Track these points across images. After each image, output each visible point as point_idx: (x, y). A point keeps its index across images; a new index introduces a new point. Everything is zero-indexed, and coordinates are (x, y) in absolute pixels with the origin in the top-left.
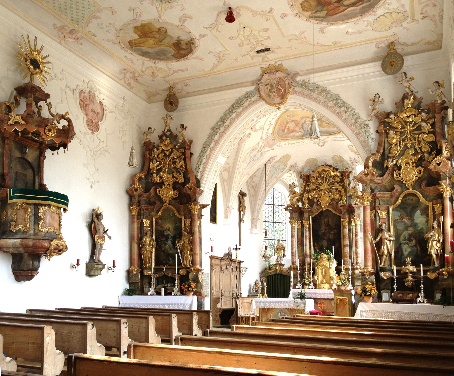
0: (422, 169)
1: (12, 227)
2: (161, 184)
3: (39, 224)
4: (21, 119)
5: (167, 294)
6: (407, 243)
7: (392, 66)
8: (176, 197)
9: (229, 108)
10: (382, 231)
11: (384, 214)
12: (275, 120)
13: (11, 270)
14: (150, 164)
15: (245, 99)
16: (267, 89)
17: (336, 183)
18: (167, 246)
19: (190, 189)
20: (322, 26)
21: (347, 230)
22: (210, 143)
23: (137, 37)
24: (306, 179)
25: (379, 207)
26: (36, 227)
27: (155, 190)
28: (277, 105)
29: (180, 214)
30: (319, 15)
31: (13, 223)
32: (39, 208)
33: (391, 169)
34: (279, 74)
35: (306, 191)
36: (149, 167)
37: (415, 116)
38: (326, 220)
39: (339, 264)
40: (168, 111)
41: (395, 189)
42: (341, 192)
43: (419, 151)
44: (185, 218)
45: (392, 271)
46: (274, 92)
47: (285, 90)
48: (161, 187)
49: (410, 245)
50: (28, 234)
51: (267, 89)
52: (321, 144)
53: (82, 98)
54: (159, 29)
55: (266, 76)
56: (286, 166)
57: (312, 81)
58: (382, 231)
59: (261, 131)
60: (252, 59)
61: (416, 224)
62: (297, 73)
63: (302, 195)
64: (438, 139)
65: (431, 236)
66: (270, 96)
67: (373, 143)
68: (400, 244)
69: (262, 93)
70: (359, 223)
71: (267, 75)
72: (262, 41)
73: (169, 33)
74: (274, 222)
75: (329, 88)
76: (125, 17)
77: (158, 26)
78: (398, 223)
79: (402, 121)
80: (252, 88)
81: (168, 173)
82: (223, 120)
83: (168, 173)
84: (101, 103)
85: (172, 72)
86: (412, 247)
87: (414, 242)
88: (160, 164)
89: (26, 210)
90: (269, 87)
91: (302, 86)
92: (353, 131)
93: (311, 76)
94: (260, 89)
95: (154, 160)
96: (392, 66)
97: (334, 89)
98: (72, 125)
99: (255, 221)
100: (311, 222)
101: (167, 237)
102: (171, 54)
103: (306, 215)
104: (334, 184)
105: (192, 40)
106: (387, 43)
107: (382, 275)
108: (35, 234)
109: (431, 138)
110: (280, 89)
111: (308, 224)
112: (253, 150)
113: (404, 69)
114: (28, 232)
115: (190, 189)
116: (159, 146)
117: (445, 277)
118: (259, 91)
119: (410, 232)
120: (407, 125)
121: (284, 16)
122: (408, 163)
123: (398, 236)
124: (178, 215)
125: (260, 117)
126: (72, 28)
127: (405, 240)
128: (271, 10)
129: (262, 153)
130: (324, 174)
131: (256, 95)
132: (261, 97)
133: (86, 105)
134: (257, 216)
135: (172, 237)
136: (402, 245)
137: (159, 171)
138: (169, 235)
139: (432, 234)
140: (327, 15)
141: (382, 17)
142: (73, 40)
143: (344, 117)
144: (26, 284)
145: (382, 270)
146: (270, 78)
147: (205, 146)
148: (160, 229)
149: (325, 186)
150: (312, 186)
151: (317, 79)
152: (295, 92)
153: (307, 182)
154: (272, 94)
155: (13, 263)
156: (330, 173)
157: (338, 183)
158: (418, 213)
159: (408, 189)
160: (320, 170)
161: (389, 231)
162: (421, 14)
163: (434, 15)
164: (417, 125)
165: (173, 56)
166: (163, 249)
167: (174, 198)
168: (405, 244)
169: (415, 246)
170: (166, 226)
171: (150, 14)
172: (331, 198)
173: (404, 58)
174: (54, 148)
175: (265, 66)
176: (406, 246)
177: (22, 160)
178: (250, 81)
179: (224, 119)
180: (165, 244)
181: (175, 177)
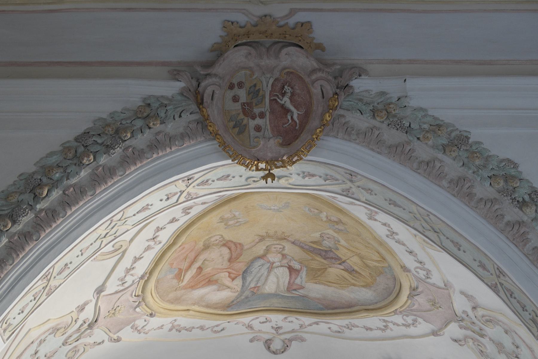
9: (66, 148)
15: (139, 123)
28: (262, 165)
34: (295, 59)
46: (262, 115)
47: (306, 117)
51: (235, 99)
52: (277, 345)
55: (238, 57)
57: (414, 103)
59: (111, 262)
62: (353, 67)
66: (241, 128)
69: (213, 112)
71: (244, 50)
75: (476, 134)
80: (170, 88)
93: (414, 84)
97: (497, 141)
110: (288, 111)
112: (55, 330)
118: (200, 103)
125: (174, 199)
129: (75, 350)
131: (187, 117)
146: (252, 64)
151: (432, 96)
152: (348, 132)
154: (252, 123)
175: (242, 19)
178: (164, 64)
179: (40, 185)
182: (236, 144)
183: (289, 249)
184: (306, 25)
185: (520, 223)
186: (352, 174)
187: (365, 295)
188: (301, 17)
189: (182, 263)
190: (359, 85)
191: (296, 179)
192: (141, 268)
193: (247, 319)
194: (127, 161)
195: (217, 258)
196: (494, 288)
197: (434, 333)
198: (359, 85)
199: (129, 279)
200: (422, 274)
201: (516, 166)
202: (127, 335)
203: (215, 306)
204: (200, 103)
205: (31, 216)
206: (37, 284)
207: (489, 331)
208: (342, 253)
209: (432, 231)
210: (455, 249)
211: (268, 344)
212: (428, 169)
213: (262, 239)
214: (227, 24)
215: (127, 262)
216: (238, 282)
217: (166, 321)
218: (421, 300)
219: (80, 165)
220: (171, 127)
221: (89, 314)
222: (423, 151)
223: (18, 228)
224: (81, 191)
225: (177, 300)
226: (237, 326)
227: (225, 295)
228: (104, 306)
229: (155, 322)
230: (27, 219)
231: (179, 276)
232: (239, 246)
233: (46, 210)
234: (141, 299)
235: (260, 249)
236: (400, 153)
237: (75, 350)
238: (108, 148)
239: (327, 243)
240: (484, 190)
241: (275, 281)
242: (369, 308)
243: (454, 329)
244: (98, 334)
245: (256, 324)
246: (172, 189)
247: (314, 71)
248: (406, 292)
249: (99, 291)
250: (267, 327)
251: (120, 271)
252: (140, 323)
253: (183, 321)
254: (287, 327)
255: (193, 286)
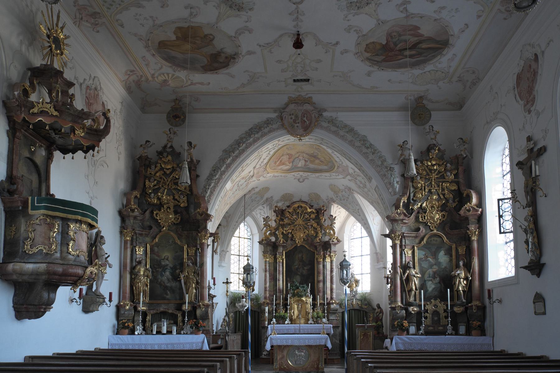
0: (446, 214)
1: (27, 247)
2: (160, 206)
3: (68, 245)
4: (52, 109)
5: (178, 333)
6: (431, 280)
7: (420, 118)
8: (178, 222)
9: (246, 133)
10: (410, 268)
11: (410, 252)
12: (273, 151)
13: (12, 305)
14: (145, 183)
15: (265, 125)
16: (291, 118)
17: (311, 220)
18: (164, 278)
19: (201, 215)
20: (372, 69)
21: (321, 266)
22: (222, 167)
23: (174, 38)
24: (280, 213)
25: (405, 245)
26: (65, 249)
27: (152, 212)
29: (181, 241)
30: (377, 58)
31: (28, 243)
32: (69, 224)
33: (416, 212)
34: (307, 107)
35: (281, 225)
36: (145, 185)
37: (439, 165)
38: (300, 256)
39: (314, 299)
40: (171, 125)
41: (421, 230)
42: (316, 229)
43: (442, 197)
44: (188, 246)
45: (420, 306)
46: (298, 123)
47: (310, 123)
48: (160, 210)
49: (434, 282)
50: (53, 257)
51: (291, 118)
52: (301, 180)
53: (88, 95)
54: (206, 36)
55: (292, 106)
56: (262, 198)
58: (410, 268)
60: (286, 87)
61: (440, 263)
63: (277, 229)
64: (462, 188)
65: (458, 274)
66: (293, 126)
67: (398, 186)
68: (425, 281)
70: (335, 259)
71: (293, 105)
72: (308, 71)
73: (214, 42)
74: (239, 256)
76: (176, 12)
77: (206, 32)
78: (423, 261)
79: (426, 168)
80: (274, 115)
81: (168, 194)
82: (238, 143)
83: (168, 194)
84: (103, 102)
85: (189, 83)
86: (436, 283)
87: (438, 279)
88: (157, 183)
89: (51, 227)
90: (293, 117)
91: (329, 122)
92: (378, 172)
94: (284, 118)
95: (152, 178)
96: (420, 118)
98: (110, 126)
99: (224, 253)
100: (284, 257)
101: (164, 268)
102: (202, 65)
103: (280, 249)
104: (309, 220)
105: (235, 55)
106: (416, 96)
107: (411, 309)
108: (62, 258)
109: (454, 187)
111: (282, 260)
113: (431, 123)
114: (53, 254)
115: (201, 215)
116: (157, 163)
117: (475, 311)
118: (282, 120)
119: (435, 270)
120: (431, 172)
121: (346, 51)
122: (434, 207)
123: (423, 272)
124: (179, 243)
126: (98, 10)
127: (429, 277)
128: (337, 43)
129: (248, 183)
130: (299, 211)
132: (283, 125)
133: (91, 104)
134: (227, 249)
135: (170, 268)
136: (427, 282)
137: (156, 191)
138: (167, 265)
139: (458, 272)
140: (384, 60)
141: (427, 73)
142: (89, 25)
143: (370, 158)
144: (29, 323)
145: (411, 304)
147: (215, 169)
148: (156, 258)
149: (300, 221)
150: (286, 221)
151: (344, 117)
152: (322, 127)
153: (281, 216)
154: (296, 125)
155: (15, 295)
156: (307, 209)
157: (313, 220)
158: (442, 253)
159: (432, 231)
160: (296, 205)
161: (414, 268)
162: (458, 77)
163: (467, 81)
164: (441, 174)
165: (202, 67)
166: (159, 280)
167: (174, 223)
168: (429, 280)
169: (439, 283)
170: (164, 255)
171: (207, 16)
172: (306, 234)
173: (432, 112)
174: (65, 151)
175: (293, 96)
176: (430, 282)
177: (29, 161)
178: (272, 108)
179: (240, 143)
180: (162, 275)
181: (176, 200)
182: (292, 133)
183: (305, 155)
184: (311, 98)
185: (367, 153)
186: (322, 139)
187: (326, 167)
188: (309, 95)
189: (276, 159)
190: (325, 114)
191: (307, 140)
192: (265, 161)
193: (293, 174)
194: (262, 136)
195: (285, 158)
196: (359, 169)
197: (343, 178)
198: (325, 114)
199: (262, 164)
200: (341, 163)
201: (366, 137)
202: (262, 179)
203: (285, 170)
204: (282, 120)
205: (238, 151)
206: (240, 169)
207: (358, 178)
208: (319, 157)
209: (344, 154)
210: (349, 159)
211: (299, 180)
212: (342, 137)
213: (298, 153)
214: (289, 98)
215: (262, 160)
216: (291, 164)
217: (272, 175)
218: (340, 169)
219: (250, 137)
220: (274, 126)
221: (252, 174)
222: (342, 133)
223: (235, 154)
224: (251, 144)
225: (274, 169)
226: (290, 175)
227: (287, 167)
228: (256, 171)
229: (269, 175)
230: (237, 152)
231: (275, 163)
232: (291, 155)
233: (242, 150)
234: (265, 169)
235: (297, 155)
236: (335, 133)
237: (248, 183)
238: (258, 132)
239: (315, 154)
240: (358, 144)
241: (301, 164)
242: (326, 171)
243: (349, 177)
244: (254, 178)
245: (296, 175)
246: (275, 143)
247: (313, 110)
248: (336, 167)
249: (254, 168)
250: (299, 176)
251: (260, 163)
252: (265, 175)
253: (276, 174)
254: (304, 175)
255: (279, 165)
